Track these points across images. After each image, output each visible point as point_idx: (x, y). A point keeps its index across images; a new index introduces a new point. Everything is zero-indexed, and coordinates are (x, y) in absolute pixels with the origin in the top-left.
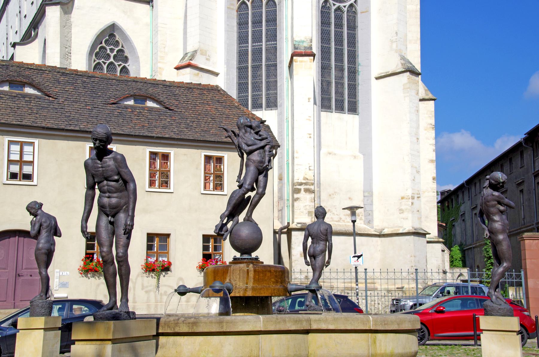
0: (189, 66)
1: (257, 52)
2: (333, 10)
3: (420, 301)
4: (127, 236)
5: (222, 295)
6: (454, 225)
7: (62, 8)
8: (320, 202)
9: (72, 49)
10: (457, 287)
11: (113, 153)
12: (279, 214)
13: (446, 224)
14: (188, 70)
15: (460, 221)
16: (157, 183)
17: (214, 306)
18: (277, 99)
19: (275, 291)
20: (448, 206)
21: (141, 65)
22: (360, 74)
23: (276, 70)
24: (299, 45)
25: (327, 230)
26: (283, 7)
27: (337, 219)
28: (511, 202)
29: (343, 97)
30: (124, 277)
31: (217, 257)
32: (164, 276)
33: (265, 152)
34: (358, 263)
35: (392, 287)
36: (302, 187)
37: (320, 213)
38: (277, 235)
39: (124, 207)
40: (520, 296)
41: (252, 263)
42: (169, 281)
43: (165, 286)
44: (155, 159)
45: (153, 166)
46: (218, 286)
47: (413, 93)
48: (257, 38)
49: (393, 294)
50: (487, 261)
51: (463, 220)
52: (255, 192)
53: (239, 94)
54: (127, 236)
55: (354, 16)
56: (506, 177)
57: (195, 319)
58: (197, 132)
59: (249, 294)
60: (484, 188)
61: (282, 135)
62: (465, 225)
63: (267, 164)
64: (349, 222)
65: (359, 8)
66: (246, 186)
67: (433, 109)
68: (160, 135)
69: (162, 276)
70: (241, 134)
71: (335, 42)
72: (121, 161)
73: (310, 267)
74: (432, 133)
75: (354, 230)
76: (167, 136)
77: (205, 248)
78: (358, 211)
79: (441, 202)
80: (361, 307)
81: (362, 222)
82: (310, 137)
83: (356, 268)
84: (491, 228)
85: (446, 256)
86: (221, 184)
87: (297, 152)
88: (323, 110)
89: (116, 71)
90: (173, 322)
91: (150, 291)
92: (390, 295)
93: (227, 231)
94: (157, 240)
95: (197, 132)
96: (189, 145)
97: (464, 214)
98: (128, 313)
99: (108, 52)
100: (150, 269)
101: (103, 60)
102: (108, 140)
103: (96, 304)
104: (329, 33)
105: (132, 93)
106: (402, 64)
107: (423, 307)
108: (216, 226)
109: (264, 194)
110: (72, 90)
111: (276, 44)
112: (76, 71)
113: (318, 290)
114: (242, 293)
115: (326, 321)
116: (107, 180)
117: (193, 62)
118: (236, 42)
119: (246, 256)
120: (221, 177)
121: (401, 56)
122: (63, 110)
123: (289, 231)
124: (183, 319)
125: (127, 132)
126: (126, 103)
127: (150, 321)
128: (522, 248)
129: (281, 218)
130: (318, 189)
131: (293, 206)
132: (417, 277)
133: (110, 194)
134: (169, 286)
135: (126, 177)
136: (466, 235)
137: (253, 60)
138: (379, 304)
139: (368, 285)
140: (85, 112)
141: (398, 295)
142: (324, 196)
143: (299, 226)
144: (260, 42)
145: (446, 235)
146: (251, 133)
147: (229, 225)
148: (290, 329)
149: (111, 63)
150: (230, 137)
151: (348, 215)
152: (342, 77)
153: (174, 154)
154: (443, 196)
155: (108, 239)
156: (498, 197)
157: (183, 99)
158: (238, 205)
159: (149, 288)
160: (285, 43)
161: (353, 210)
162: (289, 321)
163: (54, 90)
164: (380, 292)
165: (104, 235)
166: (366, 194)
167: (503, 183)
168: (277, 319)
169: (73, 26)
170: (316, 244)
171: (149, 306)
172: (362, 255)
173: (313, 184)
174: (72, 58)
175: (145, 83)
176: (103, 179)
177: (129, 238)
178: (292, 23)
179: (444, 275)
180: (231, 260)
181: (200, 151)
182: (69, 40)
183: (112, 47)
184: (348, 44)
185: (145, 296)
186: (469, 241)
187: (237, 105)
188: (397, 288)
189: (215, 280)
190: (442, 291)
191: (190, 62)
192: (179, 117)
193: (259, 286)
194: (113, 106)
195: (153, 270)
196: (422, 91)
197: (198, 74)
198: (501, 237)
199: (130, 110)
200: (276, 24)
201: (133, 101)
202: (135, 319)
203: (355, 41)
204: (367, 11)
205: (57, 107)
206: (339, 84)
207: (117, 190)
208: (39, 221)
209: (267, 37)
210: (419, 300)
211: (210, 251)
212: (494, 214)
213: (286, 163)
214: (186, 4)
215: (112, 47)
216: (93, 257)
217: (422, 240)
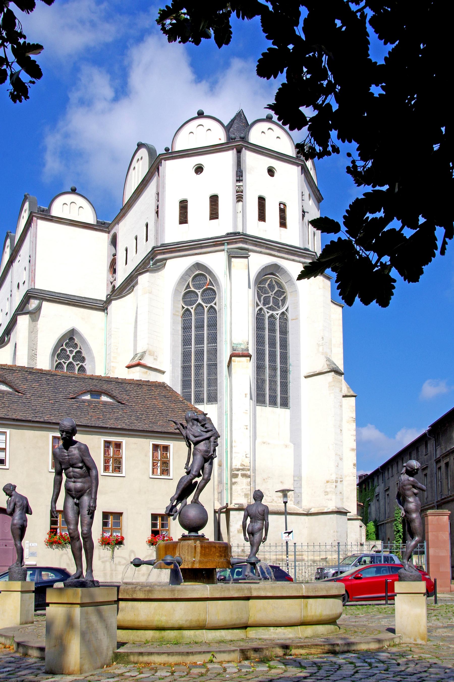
0: (138, 365)
1: (199, 353)
2: (267, 317)
3: (341, 569)
4: (90, 516)
5: (173, 567)
6: (370, 505)
7: (30, 317)
8: (255, 485)
9: (37, 351)
10: (372, 557)
11: (78, 443)
12: (218, 496)
13: (363, 503)
14: (138, 368)
15: (375, 500)
17: (165, 575)
18: (217, 394)
19: (220, 564)
20: (365, 489)
22: (291, 373)
23: (217, 369)
24: (237, 347)
25: (264, 511)
27: (272, 501)
28: (423, 486)
29: (276, 393)
30: (88, 551)
31: (164, 533)
32: (118, 549)
33: (210, 442)
34: (289, 538)
35: (317, 558)
36: (240, 473)
37: (258, 496)
38: (217, 514)
39: (88, 491)
40: (421, 563)
41: (199, 540)
42: (124, 554)
43: (119, 557)
44: (108, 447)
45: (107, 454)
46: (169, 560)
47: (338, 390)
48: (199, 340)
49: (318, 564)
50: (396, 534)
51: (378, 500)
52: (201, 478)
53: (183, 390)
54: (90, 516)
55: (286, 323)
56: (420, 465)
57: (150, 587)
58: (146, 424)
59: (197, 566)
60: (401, 474)
61: (221, 427)
62: (379, 504)
63: (212, 453)
64: (280, 503)
65: (290, 315)
66: (194, 472)
67: (354, 405)
68: (113, 426)
69: (116, 549)
70: (189, 426)
72: (85, 450)
73: (249, 542)
74: (354, 425)
75: (286, 510)
76: (119, 427)
78: (289, 494)
79: (359, 485)
80: (290, 575)
81: (292, 502)
82: (247, 429)
83: (287, 542)
84: (406, 508)
85: (363, 531)
86: (168, 470)
87: (235, 442)
88: (258, 404)
89: (74, 370)
90: (130, 590)
91: (106, 561)
92: (315, 564)
93: (176, 512)
94: (111, 518)
95: (146, 424)
96: (139, 435)
97: (378, 495)
98: (93, 581)
99: (68, 353)
100: (105, 542)
101: (63, 360)
102: (73, 432)
103: (62, 574)
104: (263, 337)
105: (89, 389)
106: (328, 365)
107: (343, 575)
108: (167, 508)
109: (210, 479)
110: (38, 387)
111: (217, 346)
112: (41, 370)
113: (257, 563)
114: (190, 565)
115: (265, 589)
116: (73, 467)
117: (142, 362)
118: (180, 344)
119: (193, 534)
120: (167, 463)
122: (30, 404)
123: (227, 511)
124: (139, 587)
126: (83, 398)
127: (112, 588)
128: (426, 523)
129: (220, 499)
130: (254, 475)
131: (231, 489)
132: (339, 549)
133: (75, 480)
134: (123, 558)
135: (89, 464)
136: (379, 513)
137: (196, 360)
138: (305, 572)
139: (297, 557)
140: (49, 406)
141: (322, 565)
142: (258, 480)
143: (237, 506)
144: (202, 344)
145: (363, 513)
146: (197, 425)
147: (179, 507)
148: (234, 596)
149: (71, 363)
150: (178, 429)
151: (280, 497)
152: (275, 376)
154: (361, 480)
155: (74, 518)
156: (413, 481)
157: (133, 394)
158: (186, 489)
159: (105, 559)
160: (224, 345)
161: (285, 493)
162: (232, 589)
163: (23, 387)
164: (306, 563)
165: (71, 514)
166: (296, 479)
167: (417, 469)
168: (222, 588)
169: (39, 332)
170: (255, 523)
171: (105, 575)
172: (292, 532)
173: (249, 470)
174: (38, 359)
175: (100, 380)
177: (92, 518)
178: (231, 328)
179: (361, 547)
180: (180, 537)
182: (36, 344)
183: (71, 349)
184: (280, 346)
185: (107, 567)
186: (382, 518)
187: (181, 400)
188: (322, 559)
189: (166, 554)
190: (359, 561)
191: (139, 362)
194: (73, 400)
195: (108, 544)
196: (345, 388)
197: (147, 372)
198: (414, 515)
200: (217, 328)
201: (89, 396)
202: (99, 587)
203: (286, 344)
204: (297, 319)
205: (25, 402)
206: (273, 382)
207: (82, 476)
209: (208, 340)
210: (340, 568)
211: (158, 528)
212: (409, 496)
213: (225, 451)
214: (137, 311)
215: (71, 349)
216: (56, 532)
217: (344, 518)
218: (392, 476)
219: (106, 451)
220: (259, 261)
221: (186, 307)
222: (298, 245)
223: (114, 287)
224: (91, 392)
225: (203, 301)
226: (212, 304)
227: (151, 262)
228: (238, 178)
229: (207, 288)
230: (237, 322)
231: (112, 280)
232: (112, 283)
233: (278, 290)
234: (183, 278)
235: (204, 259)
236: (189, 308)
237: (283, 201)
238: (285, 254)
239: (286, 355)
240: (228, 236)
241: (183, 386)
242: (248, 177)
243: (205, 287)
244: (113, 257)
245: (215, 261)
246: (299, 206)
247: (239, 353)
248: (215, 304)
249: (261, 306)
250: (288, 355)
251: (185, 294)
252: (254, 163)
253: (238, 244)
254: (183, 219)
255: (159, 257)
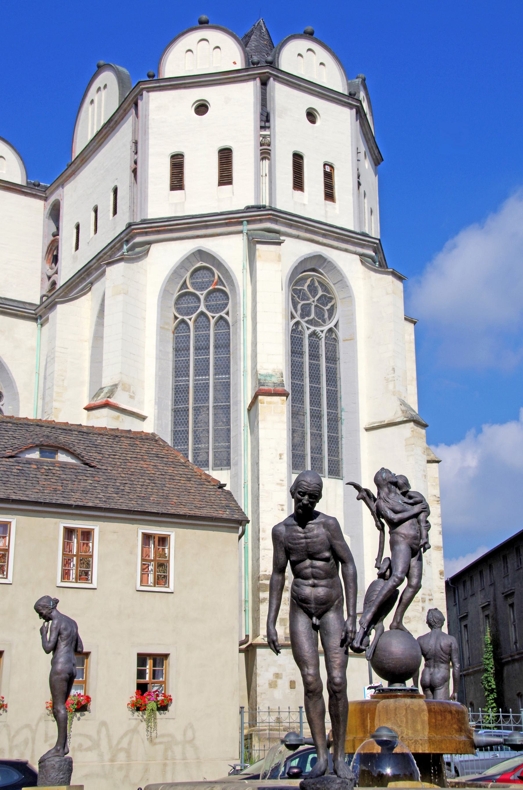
0: (106, 405)
16: (73, 574)
21: (21, 404)
22: (344, 422)
24: (265, 380)
25: (451, 646)
26: (240, 328)
33: (419, 522)
39: (337, 601)
43: (80, 735)
48: (202, 369)
50: (488, 695)
58: (131, 500)
65: (341, 334)
68: (80, 504)
71: (310, 378)
76: (90, 504)
77: (141, 674)
82: (282, 510)
86: (165, 577)
95: (131, 500)
105: (38, 442)
106: (403, 411)
111: (229, 378)
117: (112, 400)
118: (171, 374)
119: (397, 686)
121: (400, 400)
125: (33, 497)
133: (316, 581)
144: (206, 375)
146: (396, 493)
153: (100, 532)
157: (107, 451)
170: (434, 667)
175: (54, 428)
176: (305, 557)
181: (135, 526)
191: (107, 401)
192: (105, 477)
193: (438, 737)
194: (11, 460)
197: (118, 417)
199: (35, 467)
200: (229, 351)
201: (38, 453)
203: (335, 377)
204: (352, 339)
208: (56, 628)
218: (473, 595)
219: (67, 545)
220: (297, 248)
221: (180, 317)
222: (352, 228)
223: (54, 283)
224: (42, 448)
225: (208, 309)
226: (223, 314)
227: (125, 247)
228: (263, 124)
229: (215, 289)
230: (264, 341)
231: (50, 272)
232: (49, 278)
233: (322, 296)
234: (176, 273)
235: (210, 245)
236: (186, 318)
237: (330, 160)
238: (334, 240)
239: (336, 394)
240: (249, 210)
241: (174, 440)
242: (279, 123)
243: (211, 288)
244: (52, 238)
245: (230, 249)
246: (353, 170)
247: (270, 390)
248: (227, 314)
249: (298, 319)
250: (339, 395)
251: (180, 297)
252: (288, 102)
253: (263, 223)
254: (177, 182)
255: (138, 239)
